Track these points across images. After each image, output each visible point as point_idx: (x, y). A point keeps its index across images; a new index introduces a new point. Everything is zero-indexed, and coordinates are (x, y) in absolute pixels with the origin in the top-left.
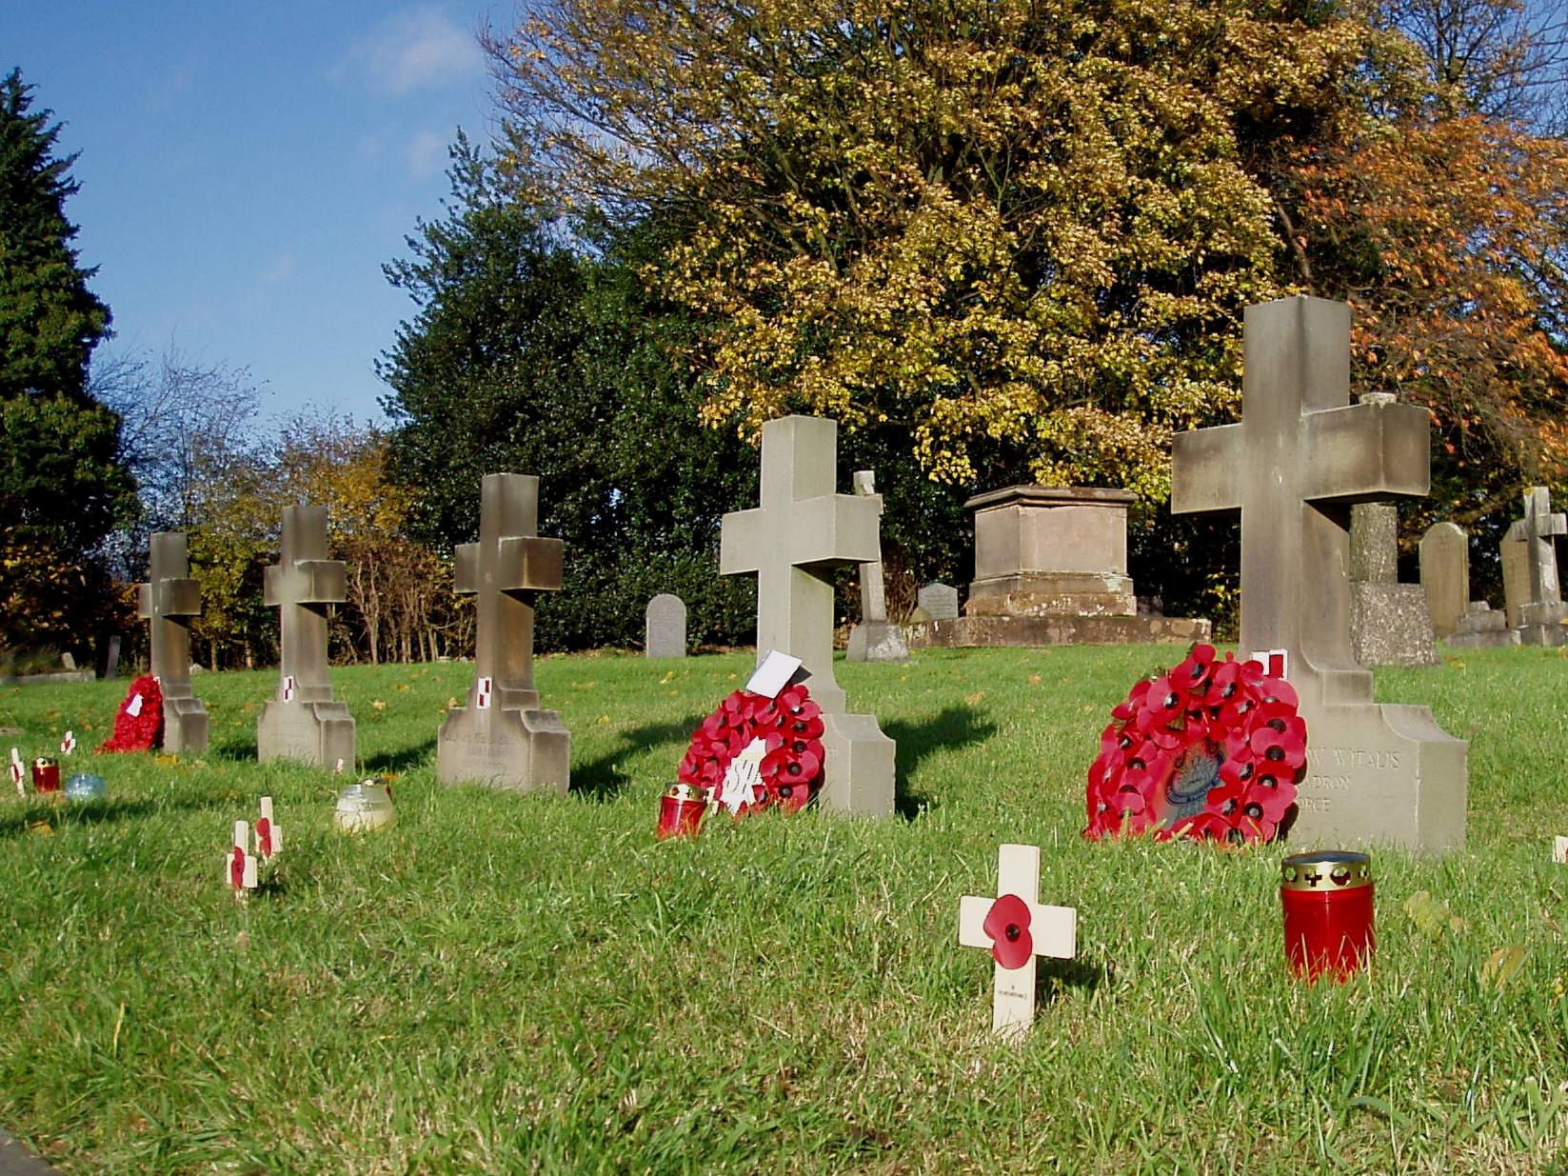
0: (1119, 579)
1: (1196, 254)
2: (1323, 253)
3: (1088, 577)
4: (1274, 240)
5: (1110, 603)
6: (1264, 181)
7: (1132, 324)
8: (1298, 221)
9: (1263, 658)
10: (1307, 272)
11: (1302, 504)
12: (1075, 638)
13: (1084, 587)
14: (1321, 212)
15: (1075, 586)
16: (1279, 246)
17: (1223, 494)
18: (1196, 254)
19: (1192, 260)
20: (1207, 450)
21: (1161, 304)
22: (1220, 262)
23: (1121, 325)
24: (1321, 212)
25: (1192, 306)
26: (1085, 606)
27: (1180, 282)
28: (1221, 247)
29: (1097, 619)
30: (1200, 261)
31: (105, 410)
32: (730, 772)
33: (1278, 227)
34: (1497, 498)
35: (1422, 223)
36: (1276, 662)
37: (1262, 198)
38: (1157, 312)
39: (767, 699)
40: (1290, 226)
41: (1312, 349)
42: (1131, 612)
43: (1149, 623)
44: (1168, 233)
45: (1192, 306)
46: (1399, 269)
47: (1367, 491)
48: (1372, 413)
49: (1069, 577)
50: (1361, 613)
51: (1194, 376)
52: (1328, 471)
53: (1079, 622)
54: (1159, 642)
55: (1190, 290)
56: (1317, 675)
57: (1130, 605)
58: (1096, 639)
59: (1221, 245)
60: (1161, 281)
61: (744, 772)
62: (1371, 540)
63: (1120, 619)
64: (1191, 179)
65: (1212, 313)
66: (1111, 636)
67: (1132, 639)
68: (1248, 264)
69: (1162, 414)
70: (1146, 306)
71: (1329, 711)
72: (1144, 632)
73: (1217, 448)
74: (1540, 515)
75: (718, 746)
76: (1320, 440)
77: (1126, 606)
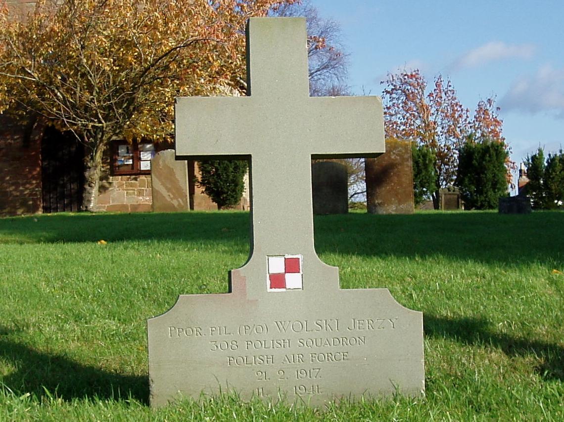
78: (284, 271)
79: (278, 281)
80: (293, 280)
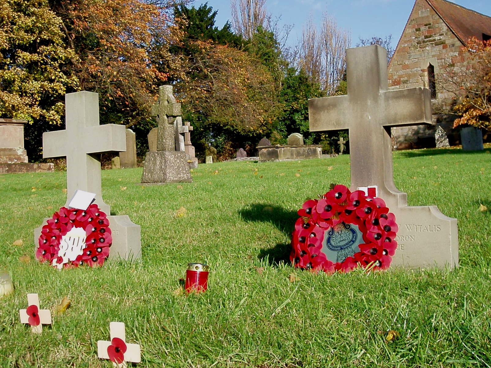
0: (21, 150)
1: (37, 38)
2: (79, 39)
3: (11, 150)
4: (62, 34)
5: (19, 159)
6: (58, 14)
7: (14, 62)
8: (69, 29)
9: (365, 189)
10: (73, 46)
11: (382, 128)
12: (8, 171)
13: (10, 153)
14: (80, 26)
15: (7, 153)
16: (63, 36)
17: (338, 123)
18: (37, 38)
19: (35, 41)
20: (329, 105)
21: (25, 56)
22: (46, 42)
23: (10, 63)
24: (80, 26)
25: (35, 57)
26: (10, 159)
27: (32, 48)
28: (45, 37)
29: (14, 164)
30: (38, 41)
31: (159, 89)
32: (62, 242)
33: (62, 30)
34: (134, 120)
35: (113, 31)
36: (372, 192)
37: (59, 20)
38: (24, 59)
39: (82, 211)
40: (66, 31)
41: (381, 67)
42: (26, 161)
43: (33, 165)
44: (26, 31)
45: (35, 57)
46: (106, 45)
47: (414, 123)
48: (418, 92)
49: (4, 150)
50: (165, 162)
51: (36, 79)
52: (396, 114)
53: (9, 165)
54: (37, 172)
55: (35, 52)
56: (394, 195)
57: (26, 160)
58: (15, 171)
59: (45, 36)
60: (24, 48)
61: (74, 242)
62: (166, 136)
63: (23, 164)
64: (33, 14)
65: (43, 60)
66: (20, 170)
67: (28, 171)
68: (53, 43)
69: (26, 92)
70: (20, 57)
71: (401, 209)
72: (32, 168)
73: (334, 105)
74: (179, 126)
75: (57, 232)
76: (390, 102)
77: (24, 159)
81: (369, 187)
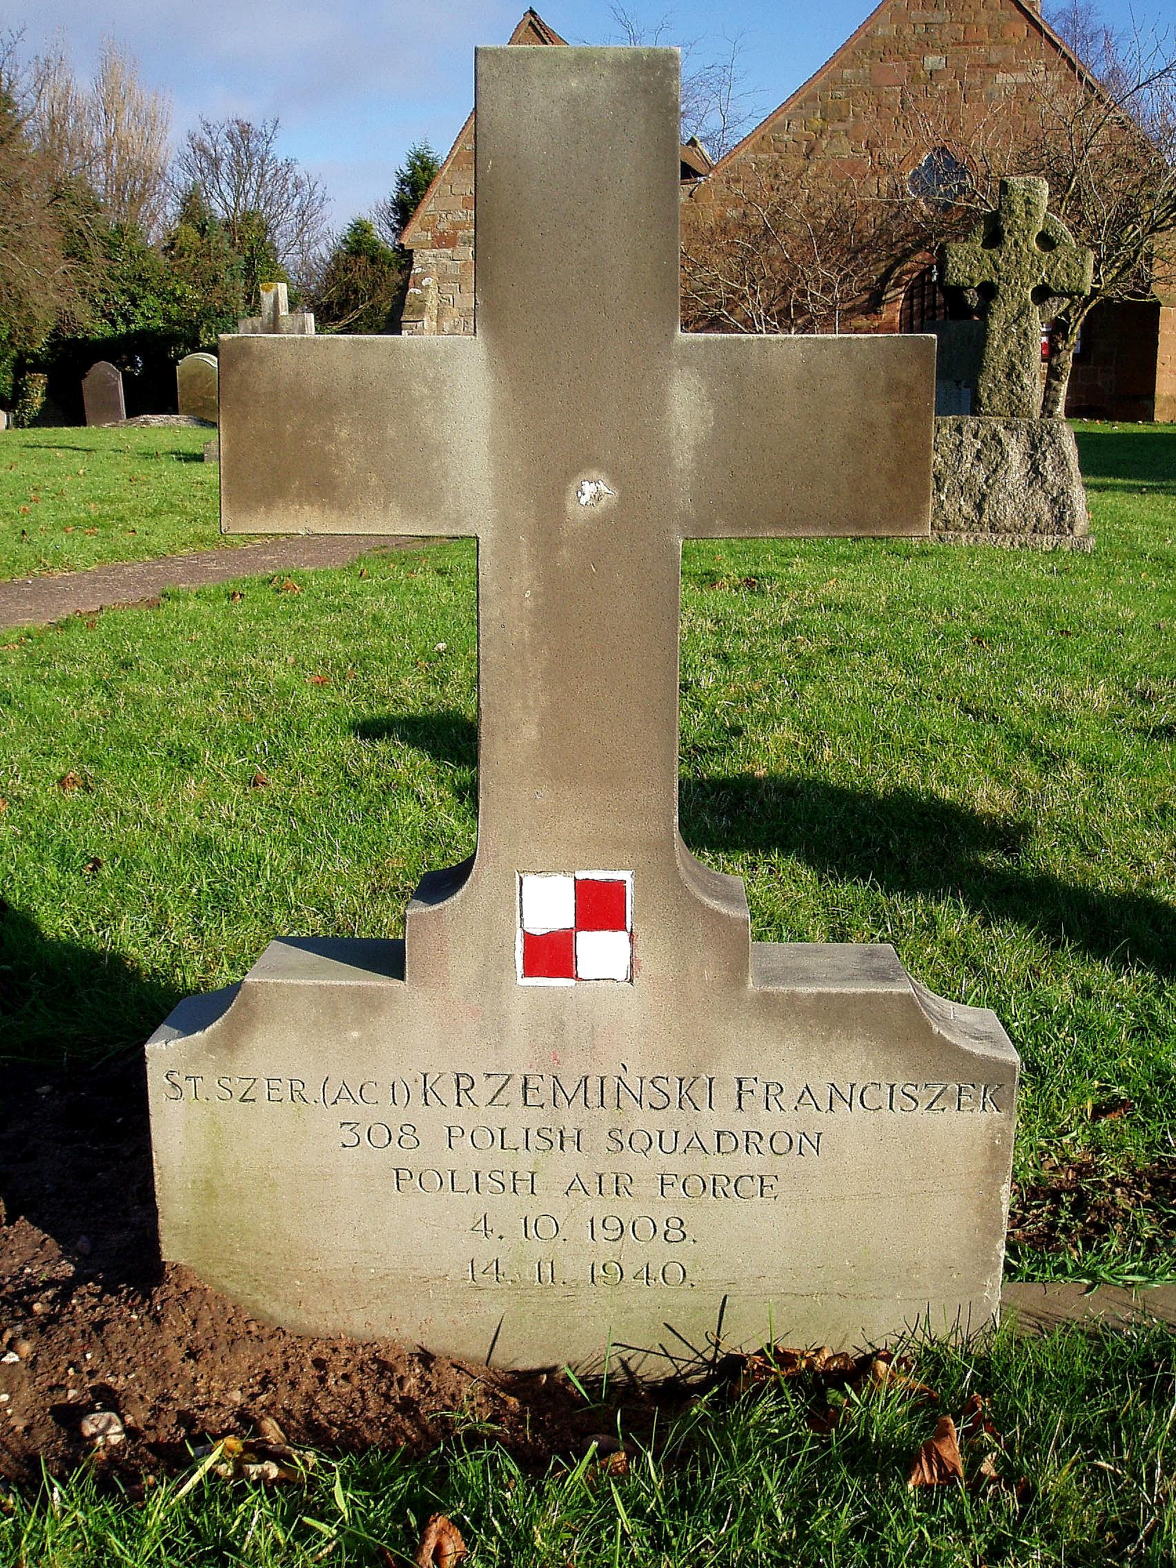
78: (570, 922)
79: (549, 955)
80: (601, 953)
81: (581, 875)
